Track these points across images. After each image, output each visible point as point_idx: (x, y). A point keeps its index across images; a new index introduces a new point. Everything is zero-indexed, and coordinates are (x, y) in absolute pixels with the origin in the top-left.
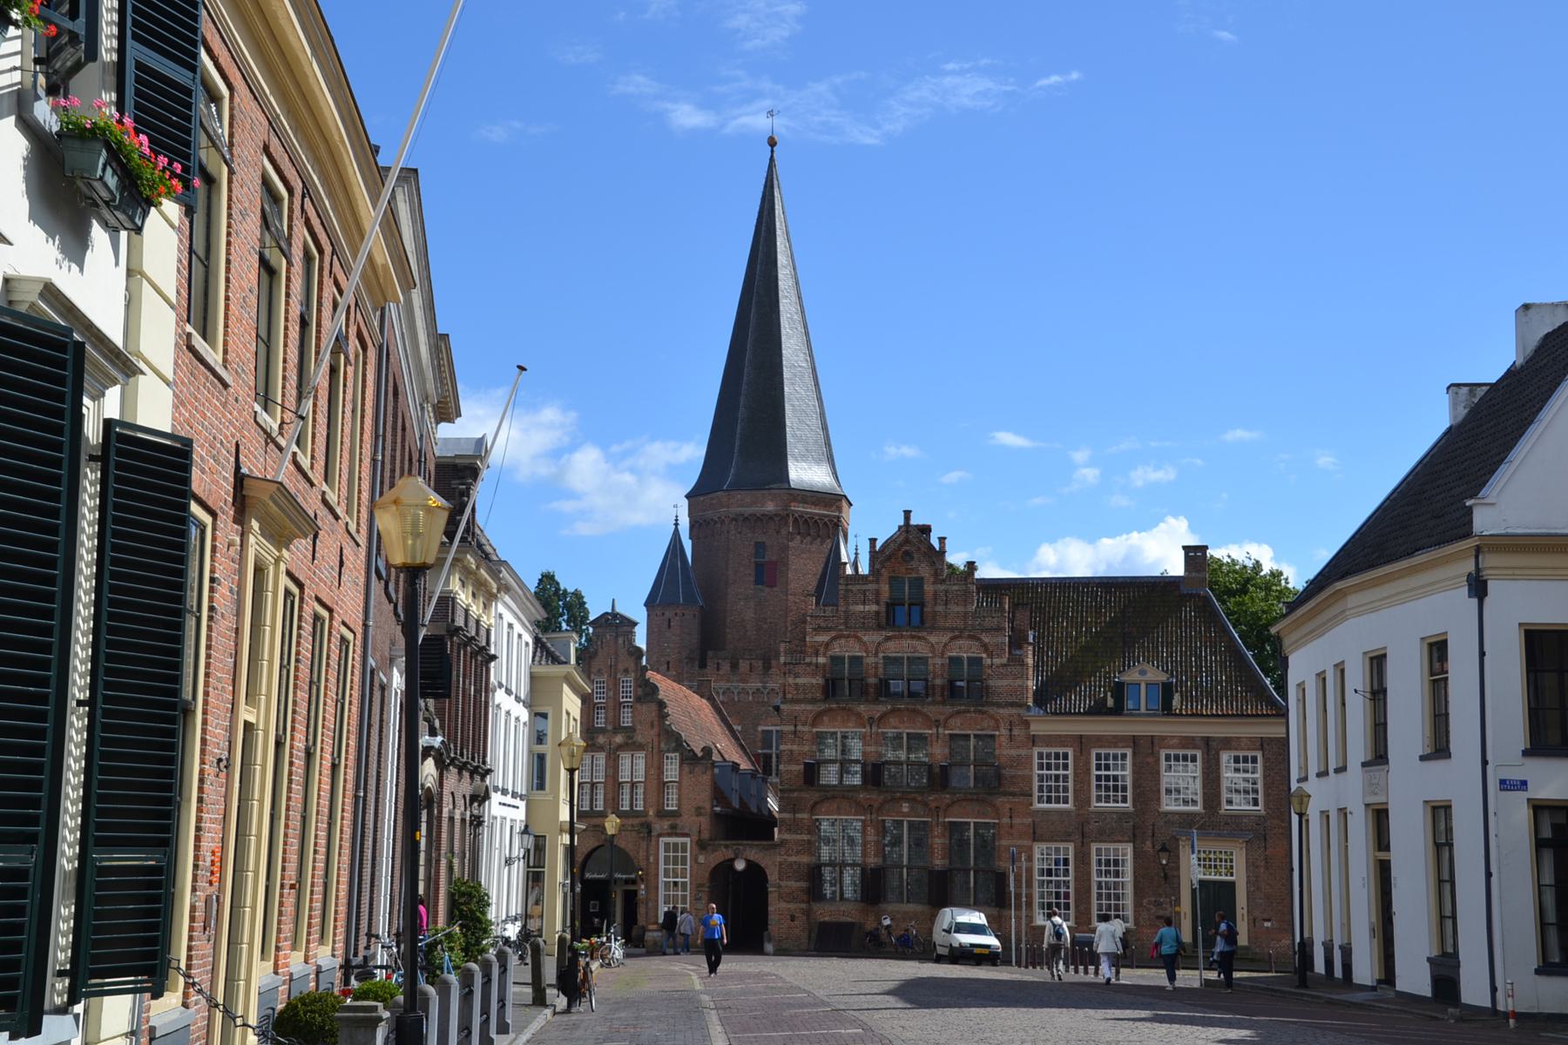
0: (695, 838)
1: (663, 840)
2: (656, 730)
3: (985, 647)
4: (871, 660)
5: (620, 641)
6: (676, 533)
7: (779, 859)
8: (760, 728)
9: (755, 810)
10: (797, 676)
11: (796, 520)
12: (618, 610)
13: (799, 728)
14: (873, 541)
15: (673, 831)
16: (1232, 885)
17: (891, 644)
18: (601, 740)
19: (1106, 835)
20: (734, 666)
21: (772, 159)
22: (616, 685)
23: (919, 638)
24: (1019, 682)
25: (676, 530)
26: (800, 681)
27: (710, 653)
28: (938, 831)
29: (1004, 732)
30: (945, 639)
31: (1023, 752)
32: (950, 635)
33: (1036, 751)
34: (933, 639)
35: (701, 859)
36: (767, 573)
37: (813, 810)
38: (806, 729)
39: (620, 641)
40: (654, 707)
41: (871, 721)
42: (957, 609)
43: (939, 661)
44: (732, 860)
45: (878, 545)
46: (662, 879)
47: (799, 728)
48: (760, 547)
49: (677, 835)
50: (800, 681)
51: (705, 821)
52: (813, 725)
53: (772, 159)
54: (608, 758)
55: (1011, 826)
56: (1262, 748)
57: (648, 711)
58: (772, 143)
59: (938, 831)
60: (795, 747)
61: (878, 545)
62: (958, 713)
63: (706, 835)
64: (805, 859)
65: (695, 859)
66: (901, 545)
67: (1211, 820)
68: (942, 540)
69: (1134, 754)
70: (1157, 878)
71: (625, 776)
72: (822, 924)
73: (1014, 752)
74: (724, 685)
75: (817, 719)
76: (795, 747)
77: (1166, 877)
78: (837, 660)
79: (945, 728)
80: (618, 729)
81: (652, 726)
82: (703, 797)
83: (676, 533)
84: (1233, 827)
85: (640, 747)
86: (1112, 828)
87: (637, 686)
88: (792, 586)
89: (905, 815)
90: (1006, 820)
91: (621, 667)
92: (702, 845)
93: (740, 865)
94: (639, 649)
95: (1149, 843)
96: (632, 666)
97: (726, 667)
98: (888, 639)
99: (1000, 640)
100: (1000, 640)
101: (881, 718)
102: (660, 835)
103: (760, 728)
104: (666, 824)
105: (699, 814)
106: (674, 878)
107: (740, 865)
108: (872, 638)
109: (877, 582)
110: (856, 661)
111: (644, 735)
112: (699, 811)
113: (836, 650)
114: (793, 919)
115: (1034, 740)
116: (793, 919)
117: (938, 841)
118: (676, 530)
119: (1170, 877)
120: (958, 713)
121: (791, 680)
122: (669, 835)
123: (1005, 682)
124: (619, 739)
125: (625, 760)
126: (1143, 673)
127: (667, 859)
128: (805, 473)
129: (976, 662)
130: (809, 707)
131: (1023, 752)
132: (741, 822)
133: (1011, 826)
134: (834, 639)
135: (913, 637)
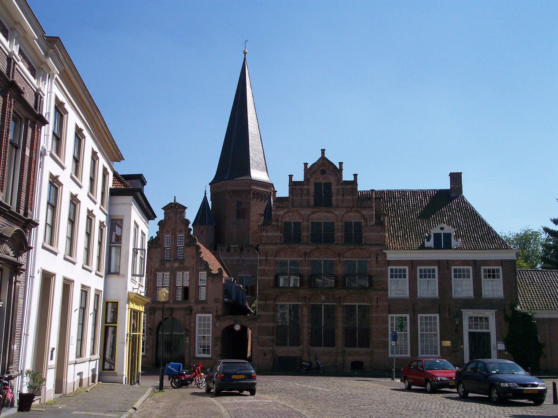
0: (215, 314)
1: (198, 315)
2: (195, 260)
3: (363, 216)
4: (305, 223)
5: (178, 216)
6: (205, 198)
7: (258, 324)
8: (239, 275)
9: (241, 303)
10: (267, 232)
11: (253, 193)
12: (177, 201)
13: (269, 258)
14: (306, 164)
15: (204, 311)
16: (488, 335)
17: (315, 216)
18: (168, 265)
19: (424, 310)
20: (228, 250)
21: (245, 58)
22: (176, 238)
23: (330, 212)
24: (381, 234)
25: (205, 196)
26: (269, 234)
27: (218, 245)
28: (340, 309)
29: (373, 259)
30: (343, 212)
31: (383, 269)
32: (345, 211)
33: (389, 268)
34: (337, 213)
35: (218, 325)
36: (242, 213)
37: (275, 299)
38: (272, 258)
39: (178, 216)
40: (194, 248)
41: (305, 254)
42: (349, 197)
43: (339, 224)
44: (233, 325)
45: (309, 166)
46: (197, 335)
47: (269, 258)
48: (239, 204)
49: (205, 313)
50: (269, 234)
51: (220, 306)
52: (276, 256)
53: (245, 58)
54: (171, 275)
55: (377, 306)
56: (501, 265)
57: (191, 251)
58: (245, 54)
59: (340, 309)
60: (266, 268)
61: (309, 166)
62: (350, 249)
63: (220, 313)
64: (271, 325)
65: (214, 325)
66: (320, 167)
67: (478, 301)
68: (341, 164)
69: (439, 269)
70: (451, 329)
71: (179, 284)
72: (281, 357)
73: (379, 269)
74: (225, 258)
75: (277, 253)
76: (266, 268)
77: (456, 331)
78: (288, 224)
79: (343, 257)
80: (176, 260)
81: (193, 258)
82: (219, 293)
83: (205, 198)
84: (489, 304)
85: (186, 269)
86: (429, 305)
87: (186, 238)
88: (251, 218)
89: (323, 302)
90: (375, 304)
91: (178, 229)
92: (217, 318)
93: (237, 328)
94: (188, 222)
95: (447, 314)
96: (183, 228)
97: (225, 251)
98: (314, 213)
99: (371, 213)
100: (371, 213)
101: (310, 253)
102: (197, 313)
103: (239, 275)
104: (200, 307)
105: (217, 302)
106: (204, 329)
107: (237, 328)
108: (306, 212)
109: (308, 185)
110: (298, 224)
111: (190, 262)
112: (216, 300)
113: (287, 219)
114: (265, 355)
115: (389, 263)
116: (265, 355)
117: (340, 315)
118: (205, 196)
119: (458, 329)
120: (350, 249)
121: (264, 234)
122: (201, 313)
123: (373, 234)
124: (176, 265)
125: (179, 274)
126: (442, 229)
127: (200, 325)
128: (257, 174)
129: (358, 225)
130: (274, 247)
131: (383, 269)
132: (234, 307)
133: (377, 306)
134: (286, 213)
135: (326, 212)
